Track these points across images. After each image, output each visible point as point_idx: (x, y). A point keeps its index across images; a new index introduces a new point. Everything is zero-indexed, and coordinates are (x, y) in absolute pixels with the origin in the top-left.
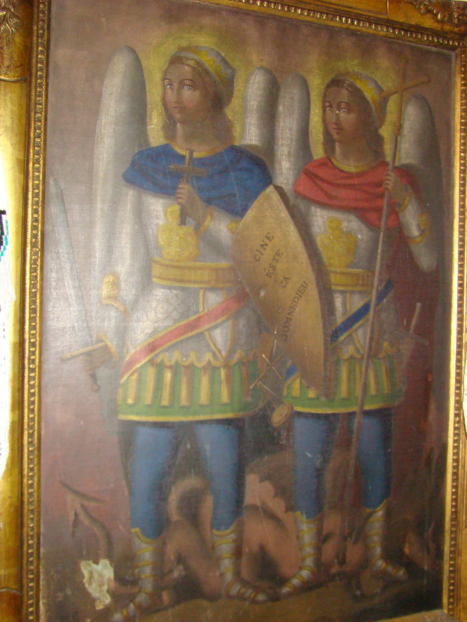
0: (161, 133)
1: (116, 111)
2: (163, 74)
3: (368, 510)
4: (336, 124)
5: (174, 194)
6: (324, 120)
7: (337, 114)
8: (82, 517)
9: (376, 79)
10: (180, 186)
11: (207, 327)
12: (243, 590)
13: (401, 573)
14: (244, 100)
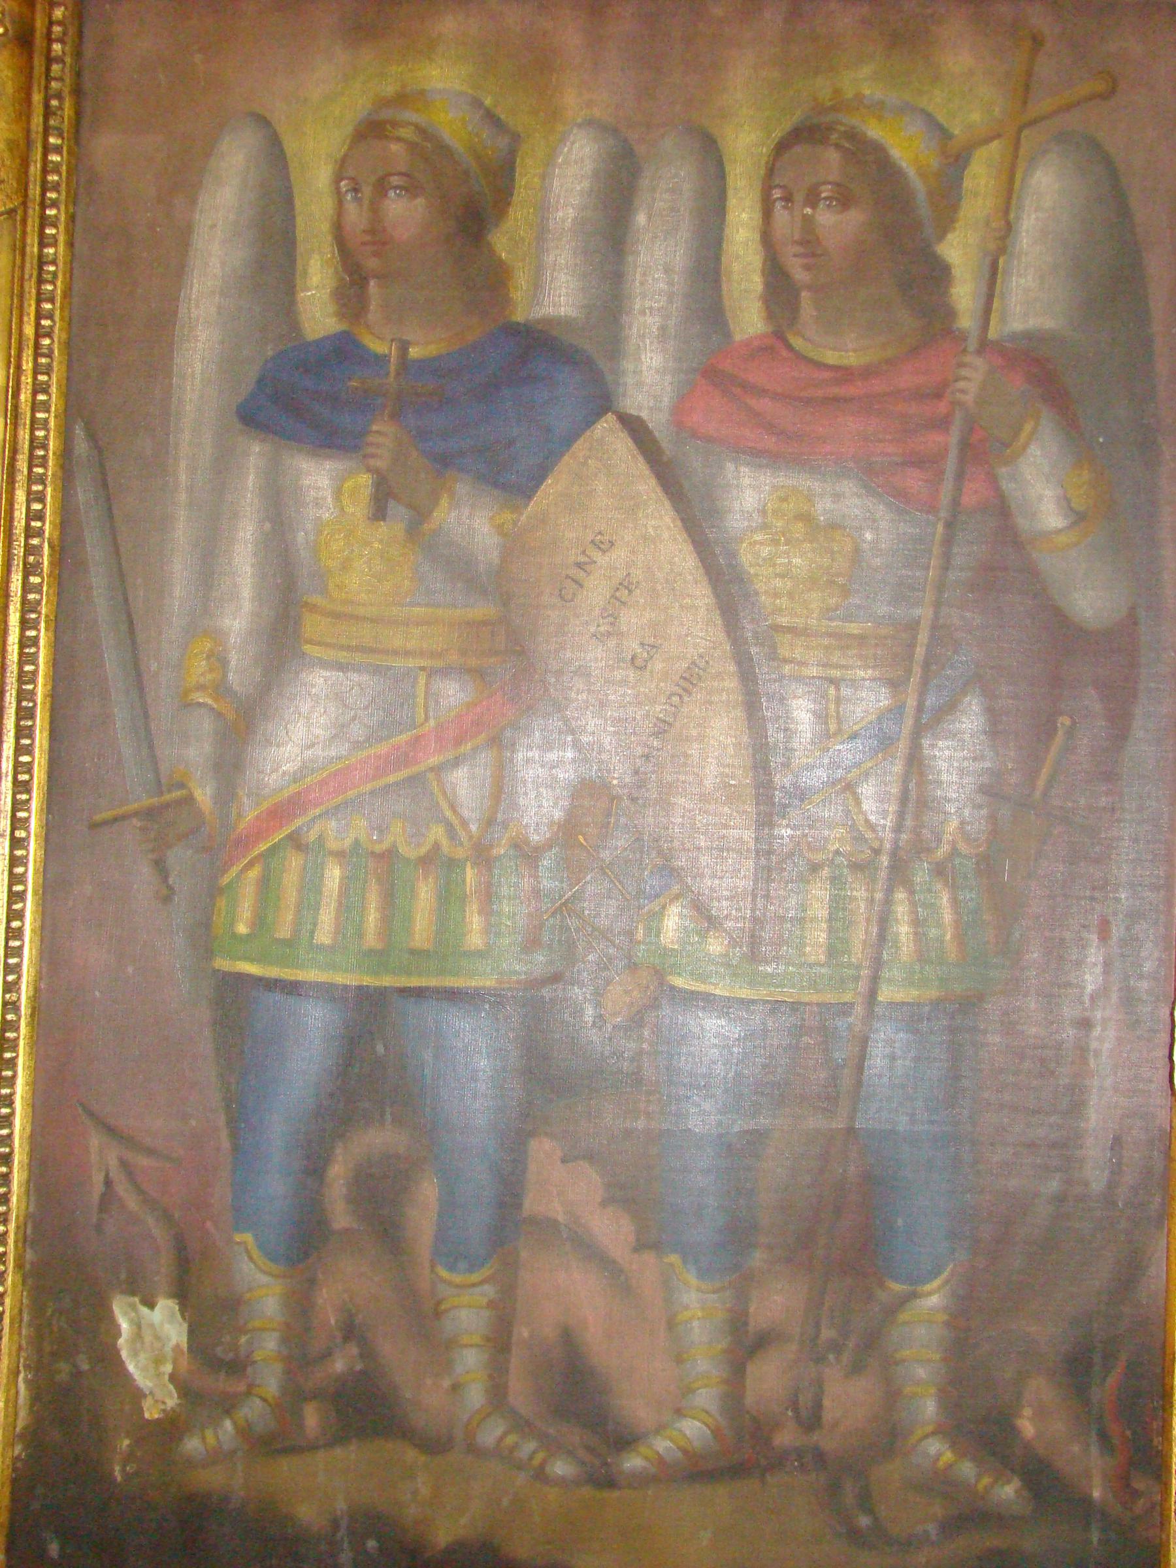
0: (331, 308)
1: (223, 264)
2: (337, 167)
3: (897, 1287)
4: (803, 242)
5: (356, 448)
6: (767, 238)
7: (805, 218)
8: (122, 1188)
9: (930, 109)
10: (374, 428)
11: (434, 760)
12: (511, 1439)
13: (1009, 1491)
14: (543, 208)
